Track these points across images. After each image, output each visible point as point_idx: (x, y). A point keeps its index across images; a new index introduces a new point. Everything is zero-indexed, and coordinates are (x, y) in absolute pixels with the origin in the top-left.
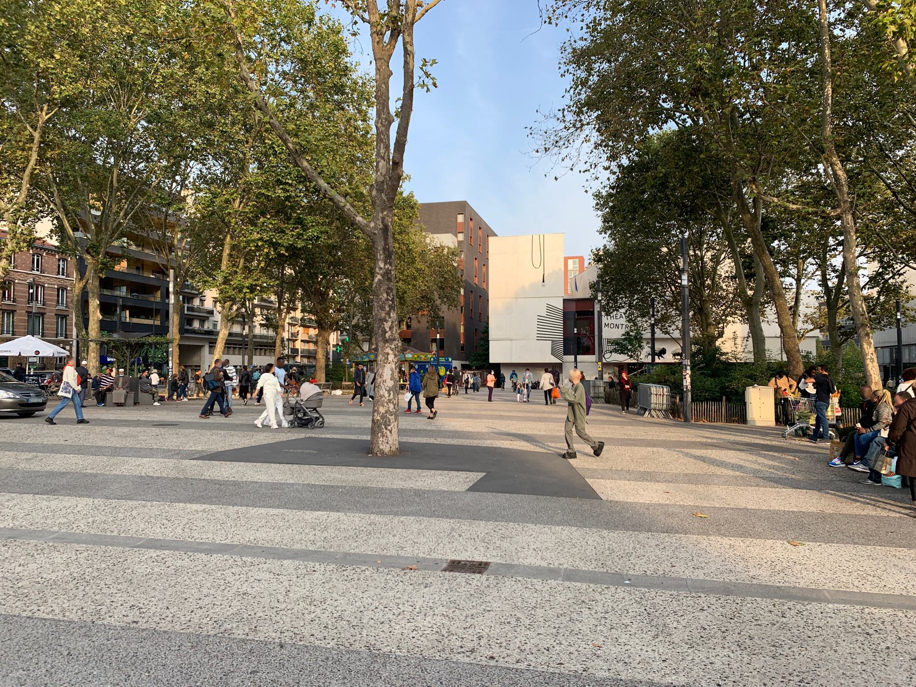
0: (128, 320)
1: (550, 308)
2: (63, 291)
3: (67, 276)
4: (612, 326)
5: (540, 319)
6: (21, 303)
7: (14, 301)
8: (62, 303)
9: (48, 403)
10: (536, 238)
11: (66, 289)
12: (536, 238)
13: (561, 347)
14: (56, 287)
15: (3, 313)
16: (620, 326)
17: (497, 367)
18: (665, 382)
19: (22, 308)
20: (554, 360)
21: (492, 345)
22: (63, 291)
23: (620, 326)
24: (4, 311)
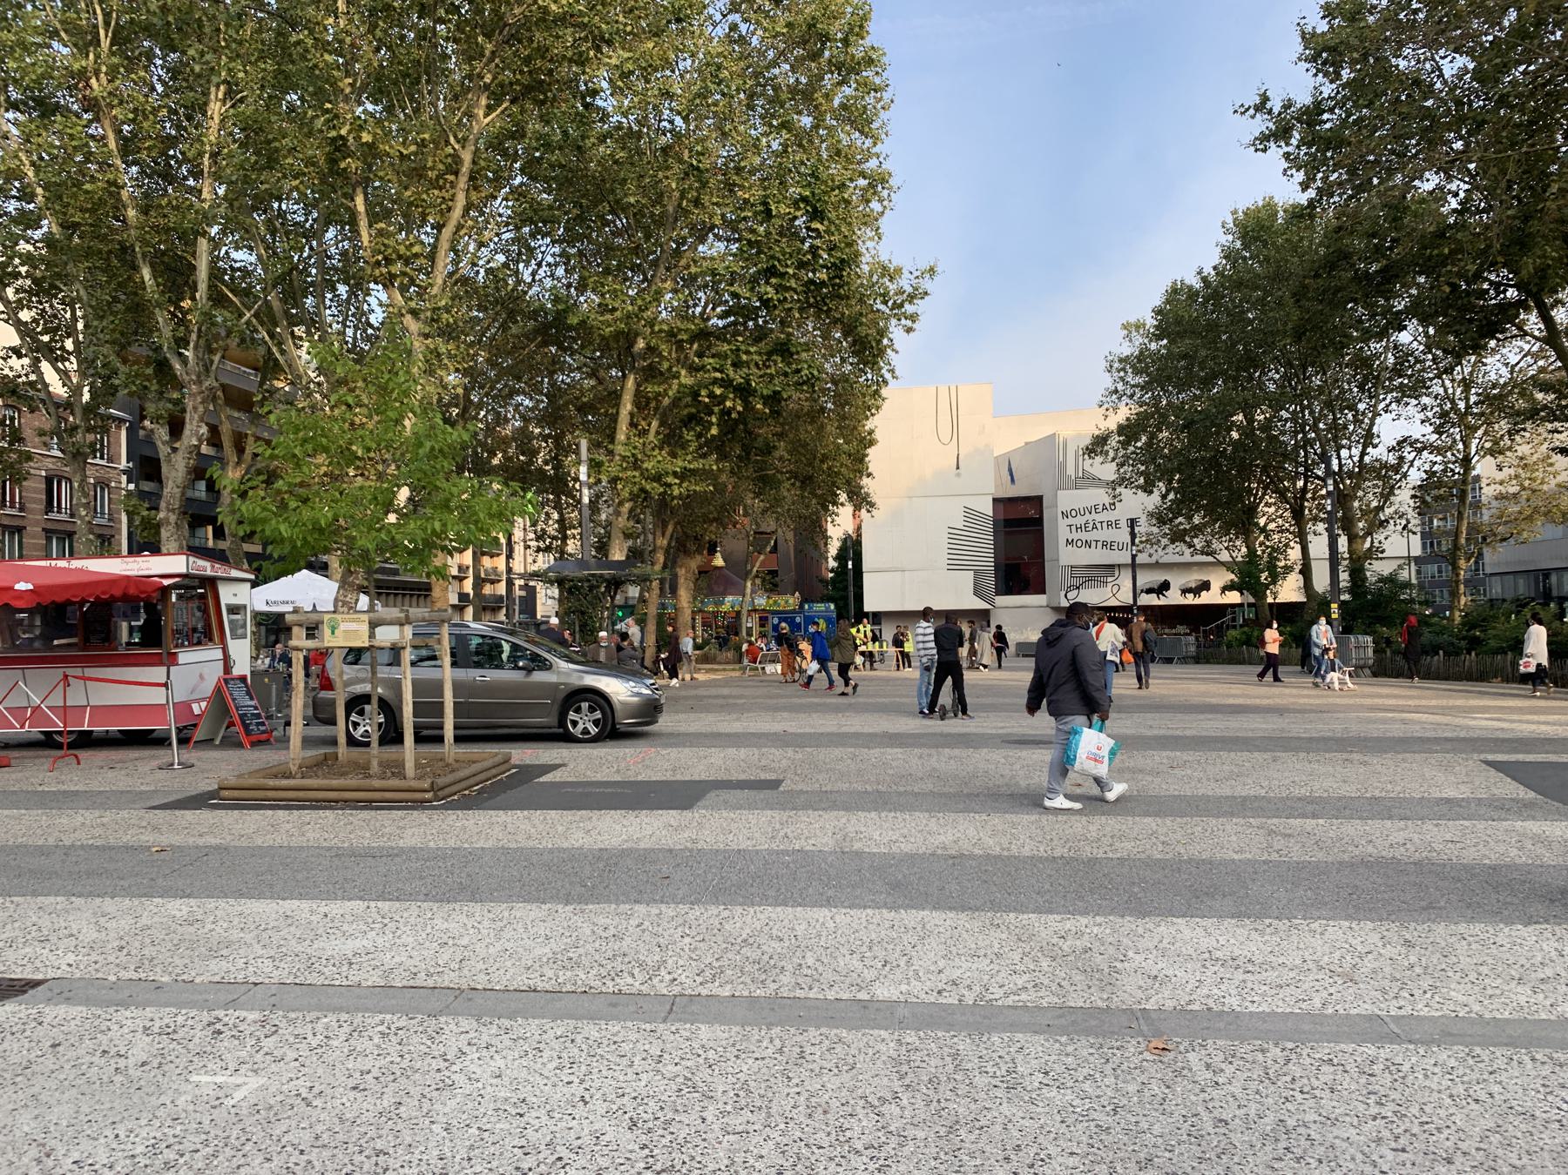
0: (211, 543)
1: (968, 511)
2: (102, 490)
3: (110, 460)
4: (1079, 544)
5: (953, 534)
6: (32, 511)
7: (21, 509)
8: (103, 513)
9: (665, 722)
10: (943, 391)
11: (108, 486)
12: (943, 391)
13: (990, 582)
14: (43, 473)
15: (49, 540)
16: (1094, 544)
17: (877, 618)
18: (88, 1000)
19: (37, 523)
20: (980, 604)
21: (868, 580)
22: (102, 490)
23: (1094, 544)
24: (5, 527)
